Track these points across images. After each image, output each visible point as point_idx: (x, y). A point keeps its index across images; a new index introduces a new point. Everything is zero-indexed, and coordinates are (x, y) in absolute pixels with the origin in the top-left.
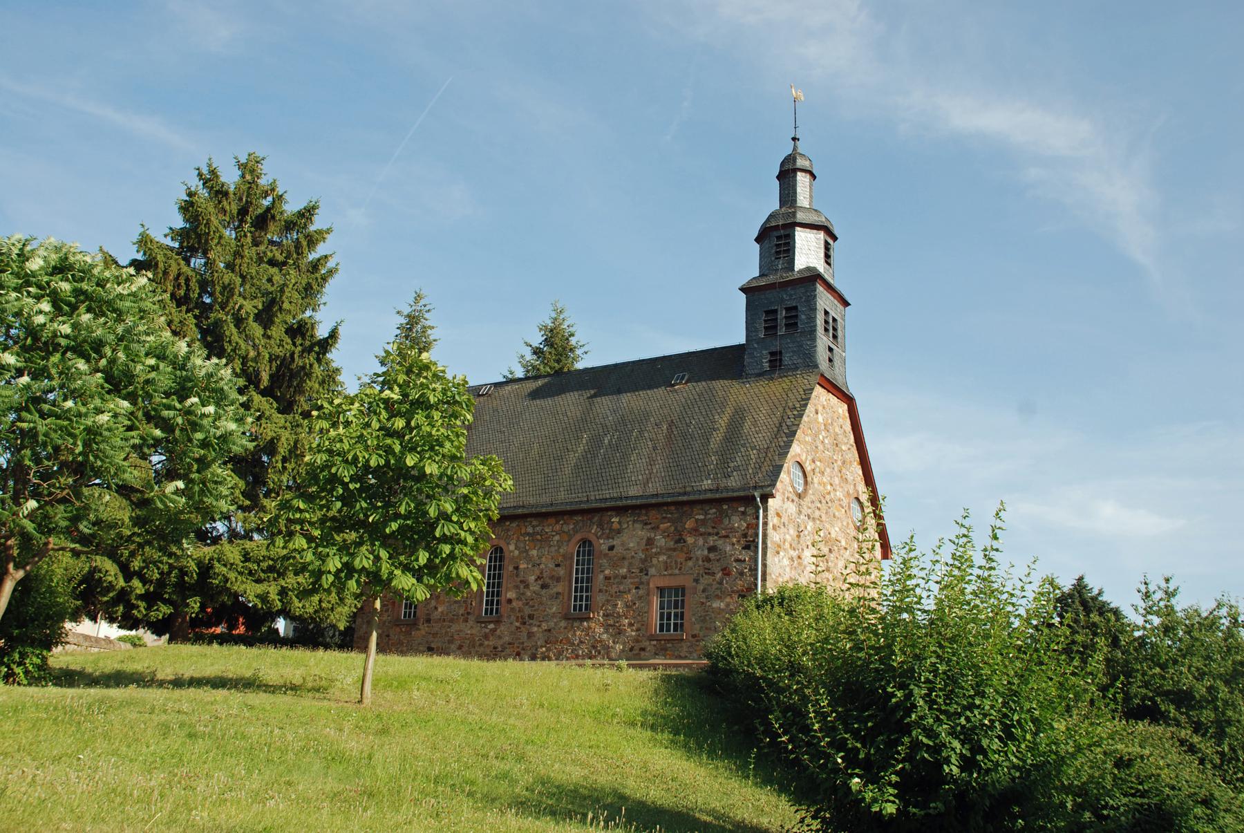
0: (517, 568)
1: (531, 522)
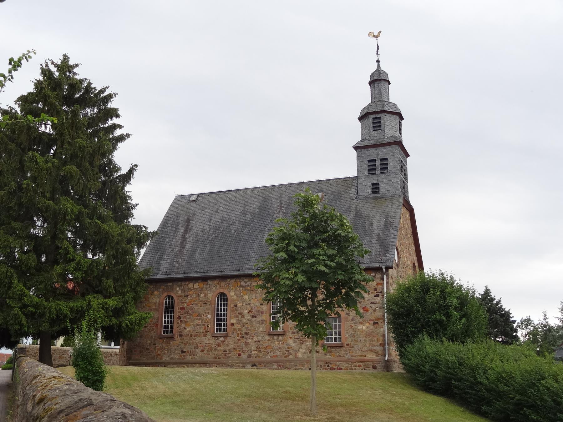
0: (236, 306)
1: (244, 279)
